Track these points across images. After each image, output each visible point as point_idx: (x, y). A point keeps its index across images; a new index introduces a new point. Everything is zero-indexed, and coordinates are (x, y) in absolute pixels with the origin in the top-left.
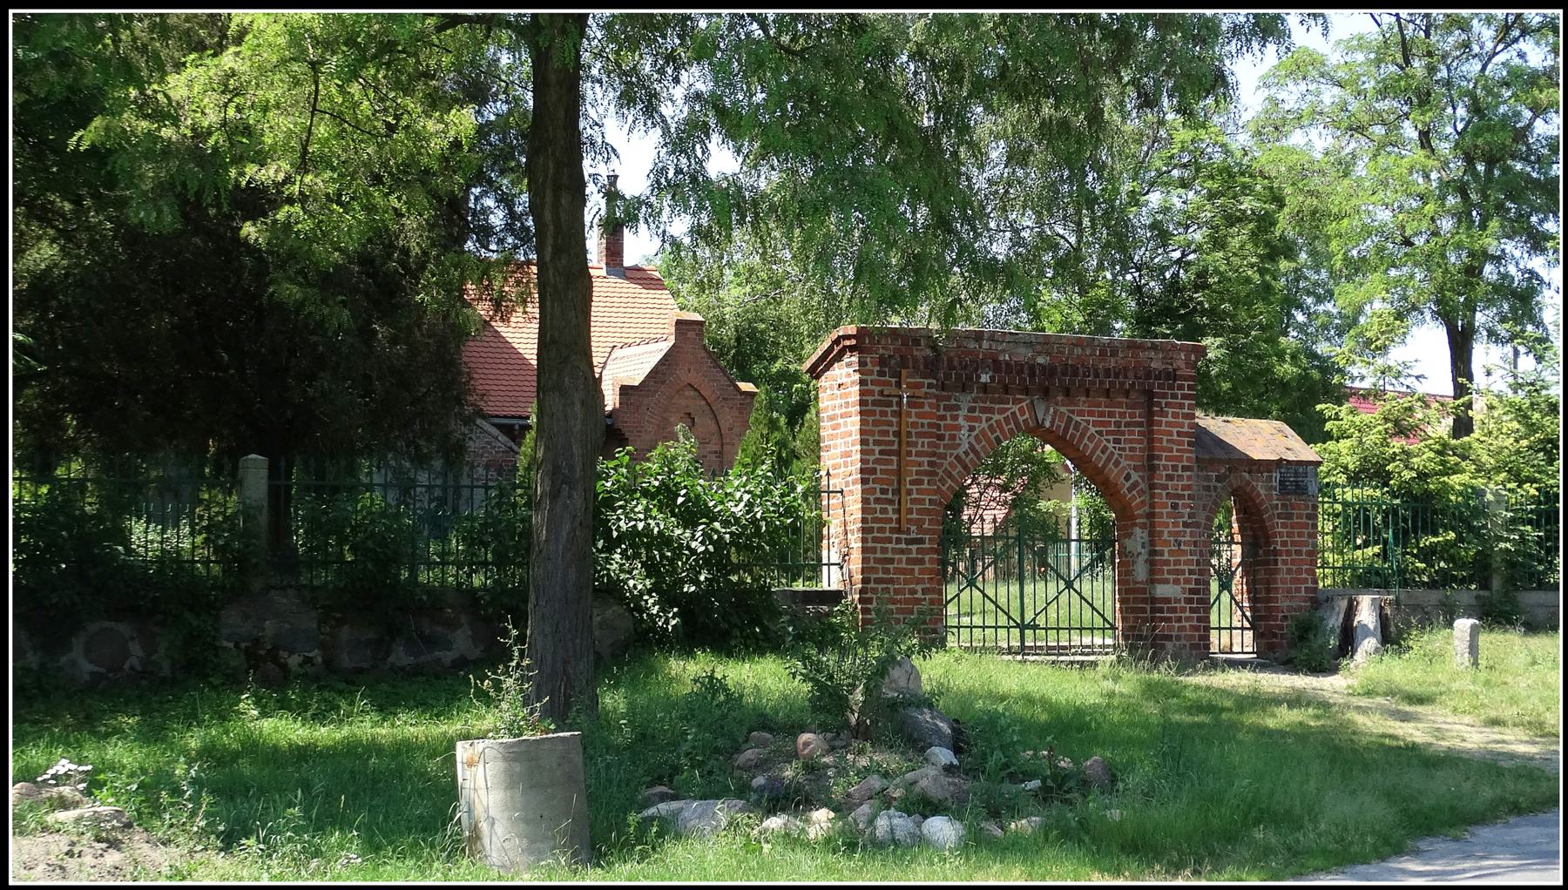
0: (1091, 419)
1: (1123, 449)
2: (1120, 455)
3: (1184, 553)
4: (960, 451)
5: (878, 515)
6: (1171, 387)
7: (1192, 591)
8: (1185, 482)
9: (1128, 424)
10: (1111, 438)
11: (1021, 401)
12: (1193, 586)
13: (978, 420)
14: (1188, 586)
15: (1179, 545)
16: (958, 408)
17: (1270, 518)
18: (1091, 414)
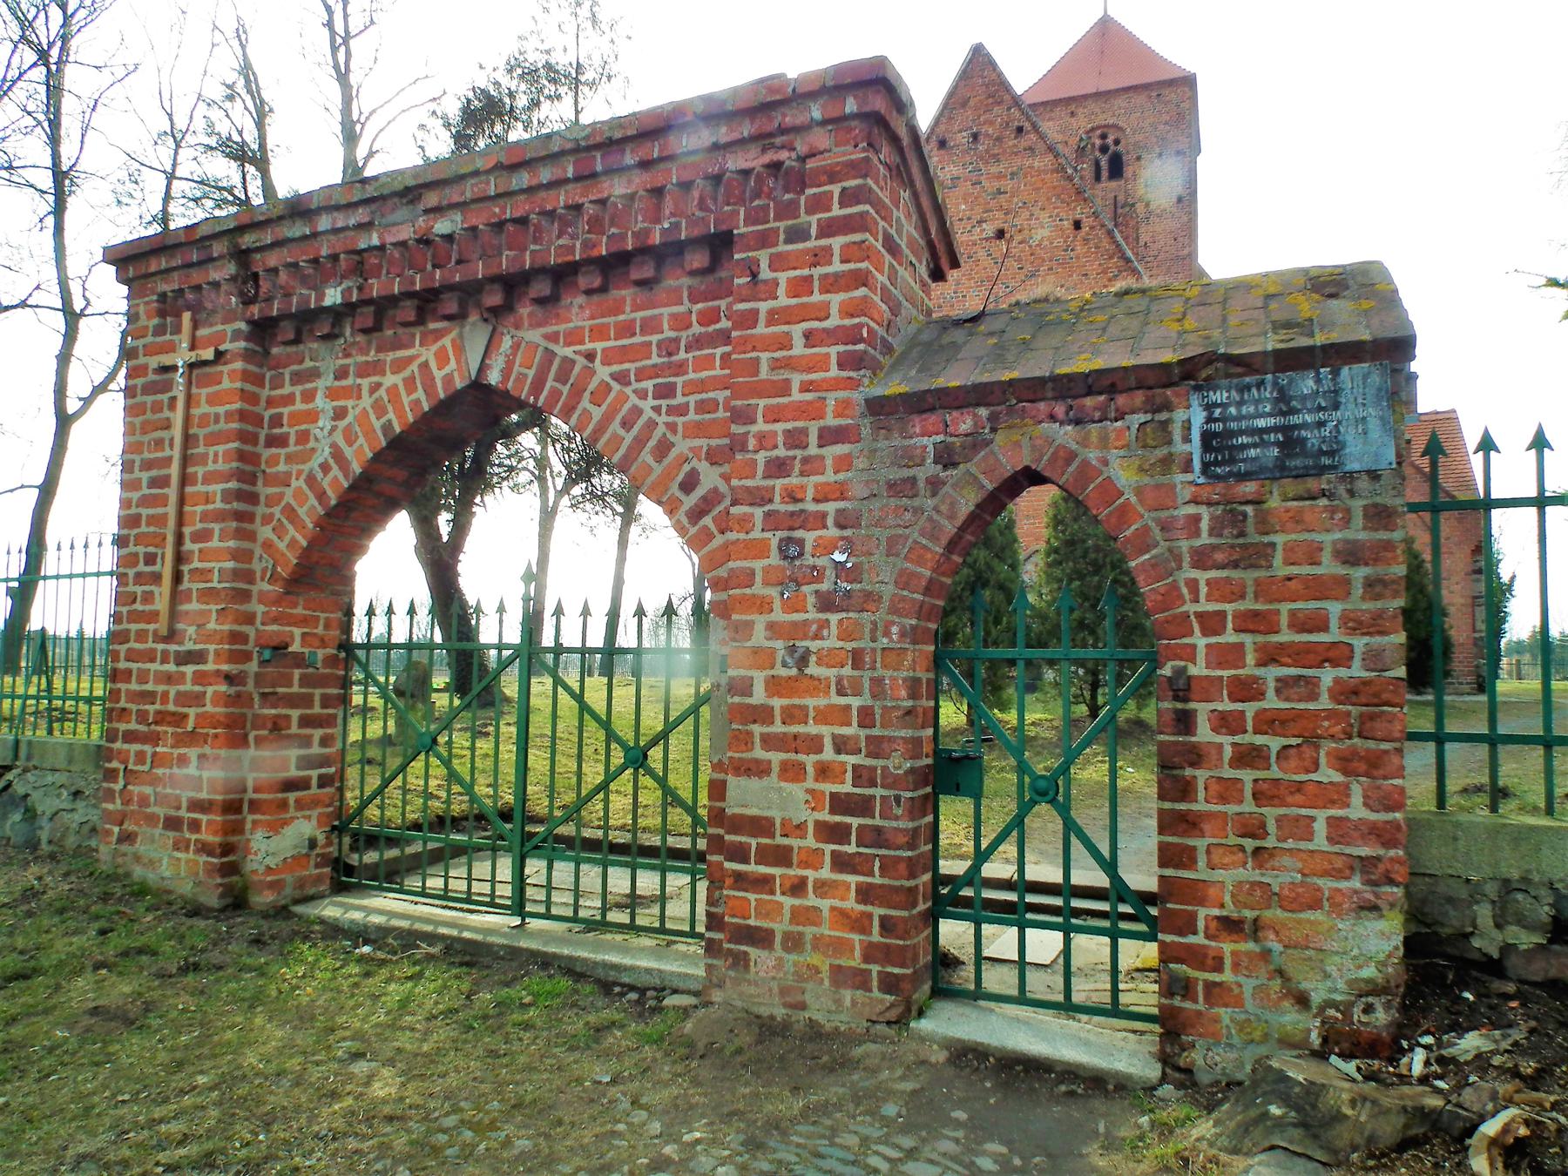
0: (599, 346)
1: (681, 410)
2: (672, 427)
3: (818, 686)
4: (314, 464)
5: (138, 606)
6: (788, 211)
7: (840, 804)
8: (830, 477)
9: (697, 343)
10: (649, 385)
11: (439, 335)
12: (847, 787)
13: (356, 392)
14: (829, 788)
15: (803, 661)
16: (314, 374)
17: (1159, 569)
18: (599, 333)
